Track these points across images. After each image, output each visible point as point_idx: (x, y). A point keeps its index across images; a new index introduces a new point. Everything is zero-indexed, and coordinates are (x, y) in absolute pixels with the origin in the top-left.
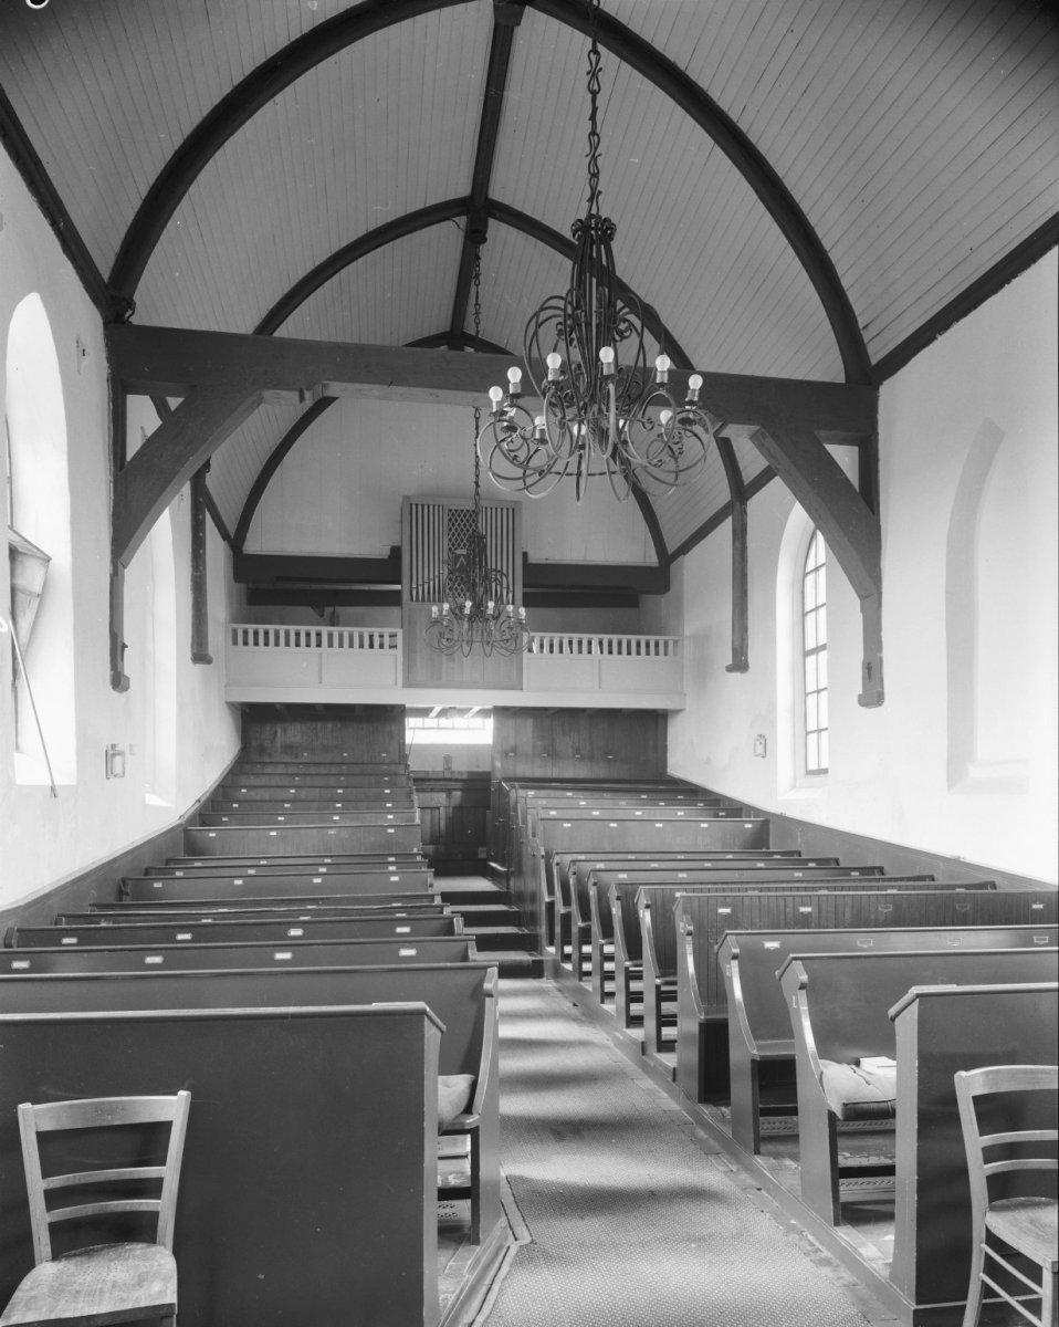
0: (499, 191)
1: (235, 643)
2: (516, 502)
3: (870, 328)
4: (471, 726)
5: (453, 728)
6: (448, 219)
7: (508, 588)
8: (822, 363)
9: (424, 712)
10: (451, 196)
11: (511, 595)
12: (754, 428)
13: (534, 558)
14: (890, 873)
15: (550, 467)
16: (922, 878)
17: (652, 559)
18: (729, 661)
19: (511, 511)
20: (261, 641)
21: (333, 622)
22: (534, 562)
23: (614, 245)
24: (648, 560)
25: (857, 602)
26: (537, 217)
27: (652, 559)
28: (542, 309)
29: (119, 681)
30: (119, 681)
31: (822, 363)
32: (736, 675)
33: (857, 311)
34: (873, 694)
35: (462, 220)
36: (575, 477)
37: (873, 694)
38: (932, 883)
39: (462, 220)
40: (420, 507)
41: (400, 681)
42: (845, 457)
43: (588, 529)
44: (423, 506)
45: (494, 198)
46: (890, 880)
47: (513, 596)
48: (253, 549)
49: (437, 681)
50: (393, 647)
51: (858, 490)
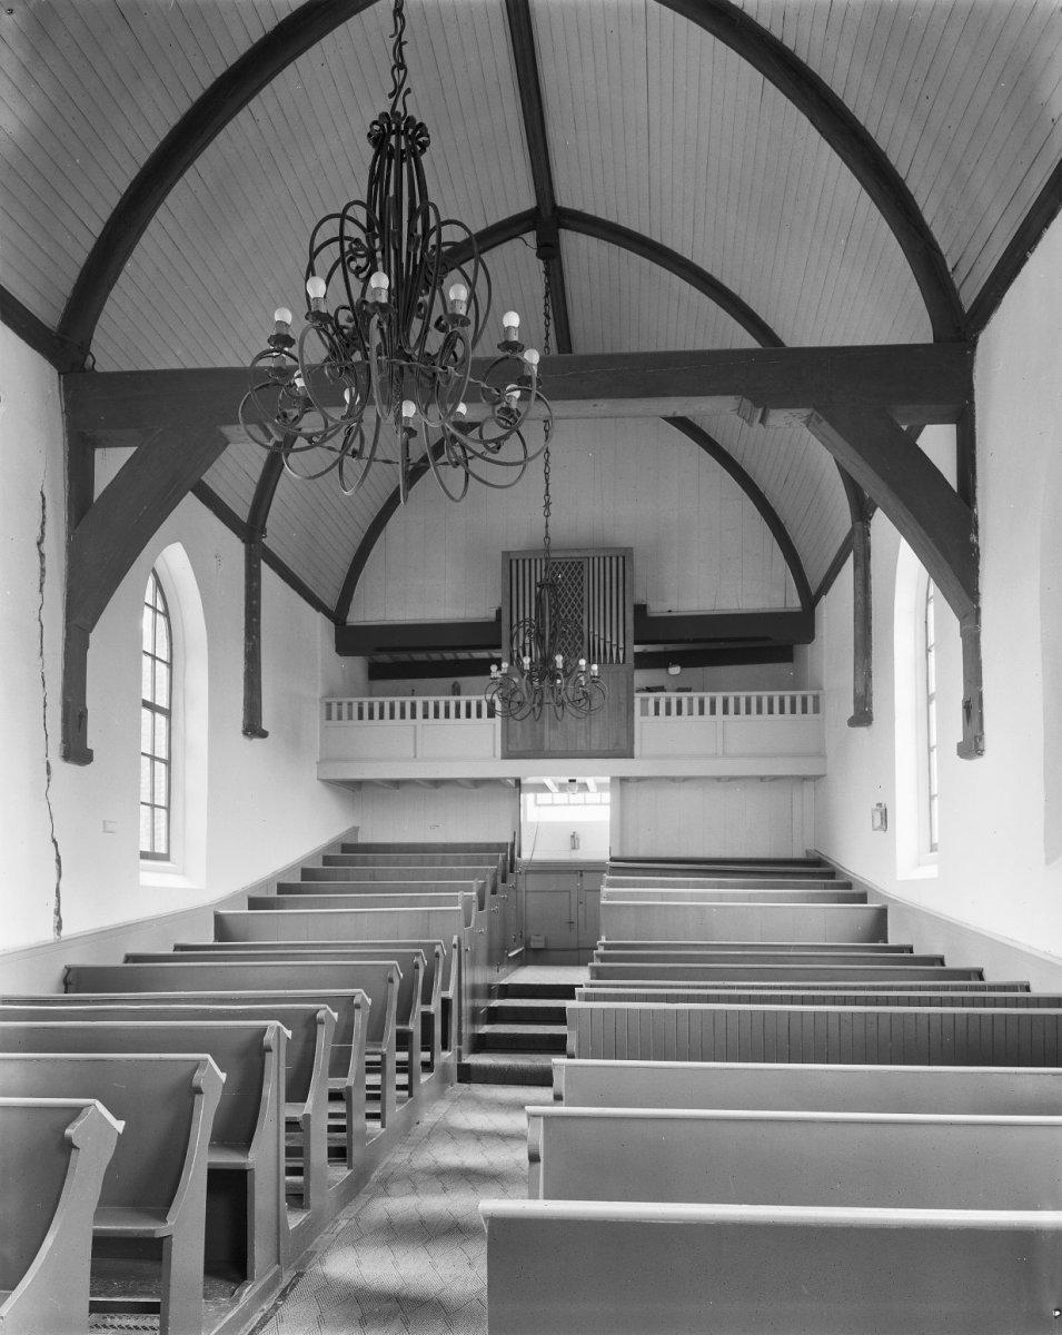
0: (566, 198)
1: (329, 718)
2: (626, 549)
3: (960, 268)
4: (572, 802)
5: (552, 805)
6: (516, 236)
7: (605, 642)
8: (902, 319)
9: (543, 788)
10: (515, 210)
11: (621, 653)
12: (805, 412)
13: (657, 608)
14: (990, 979)
15: (325, 438)
16: (1013, 988)
17: (795, 603)
18: (851, 713)
19: (621, 559)
20: (355, 714)
21: (456, 691)
22: (655, 615)
23: (424, 158)
24: (789, 605)
25: (957, 623)
26: (612, 219)
27: (795, 603)
28: (313, 255)
29: (76, 750)
30: (76, 750)
31: (902, 319)
32: (861, 731)
33: (944, 248)
34: (972, 746)
35: (531, 237)
36: (379, 455)
37: (972, 746)
38: (1026, 994)
39: (531, 237)
40: (521, 562)
41: (499, 752)
42: (937, 443)
43: (723, 574)
44: (524, 561)
45: (564, 206)
46: (993, 988)
47: (624, 654)
48: (355, 619)
49: (537, 752)
50: (491, 714)
51: (954, 486)
